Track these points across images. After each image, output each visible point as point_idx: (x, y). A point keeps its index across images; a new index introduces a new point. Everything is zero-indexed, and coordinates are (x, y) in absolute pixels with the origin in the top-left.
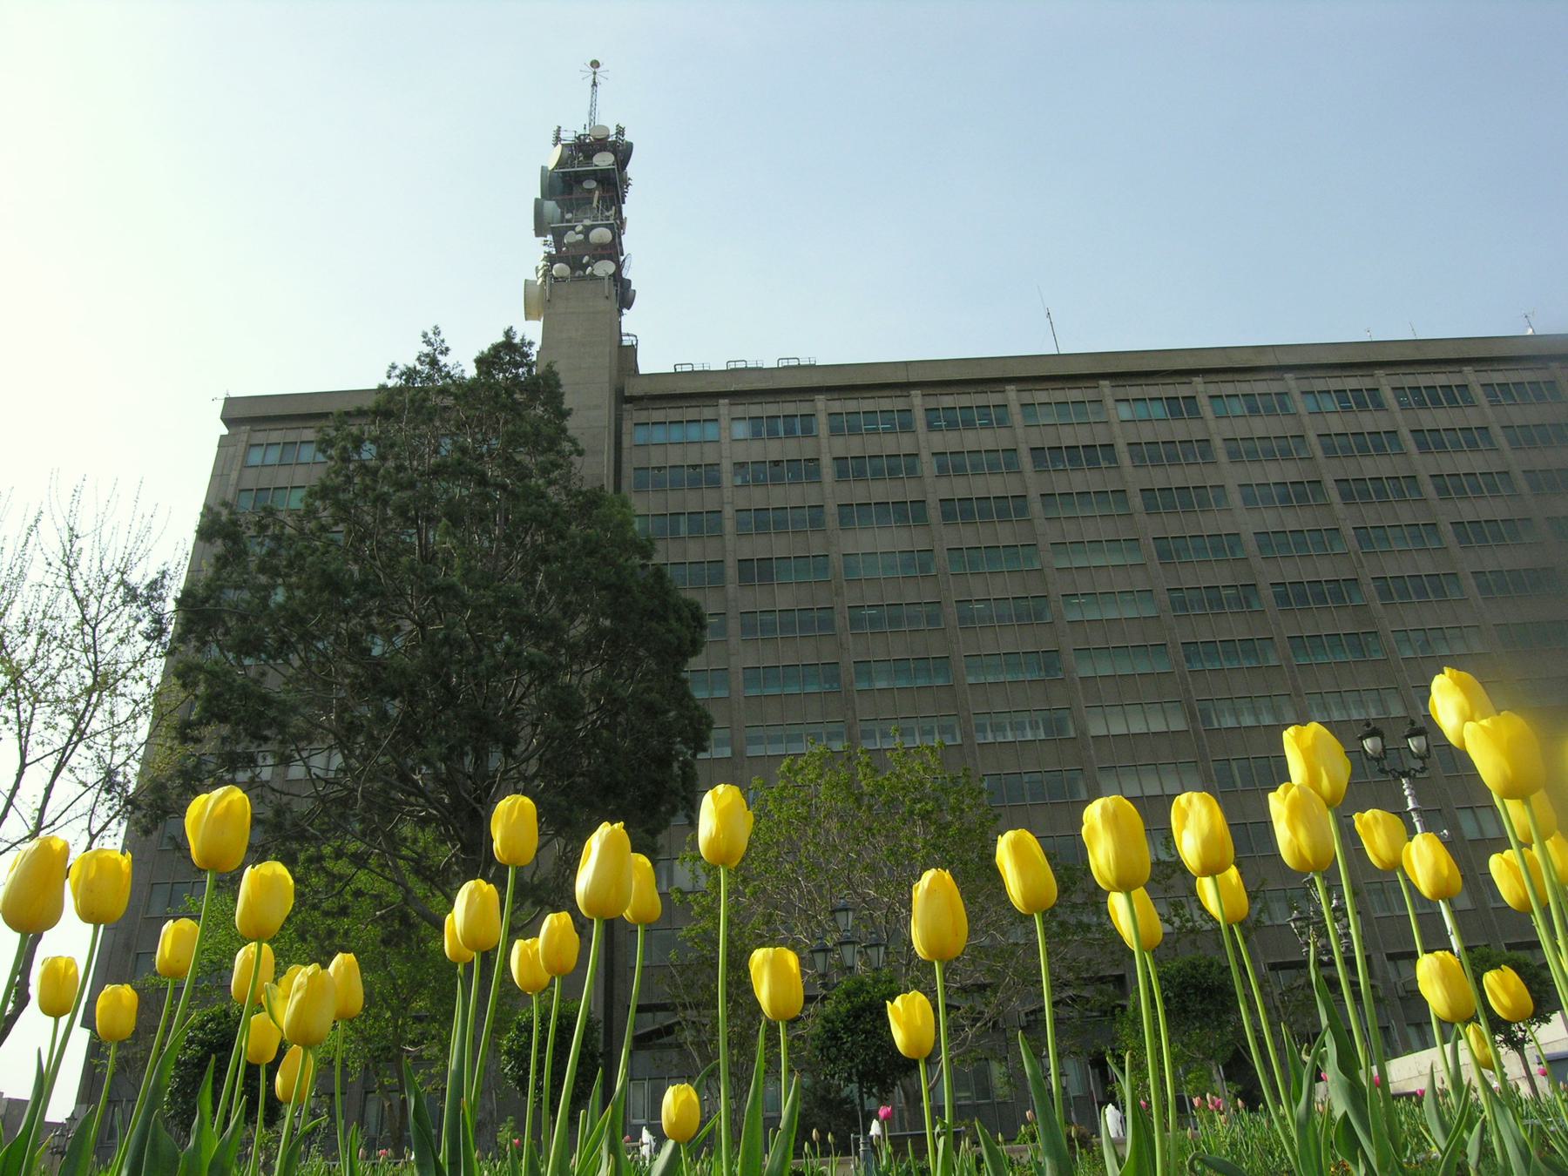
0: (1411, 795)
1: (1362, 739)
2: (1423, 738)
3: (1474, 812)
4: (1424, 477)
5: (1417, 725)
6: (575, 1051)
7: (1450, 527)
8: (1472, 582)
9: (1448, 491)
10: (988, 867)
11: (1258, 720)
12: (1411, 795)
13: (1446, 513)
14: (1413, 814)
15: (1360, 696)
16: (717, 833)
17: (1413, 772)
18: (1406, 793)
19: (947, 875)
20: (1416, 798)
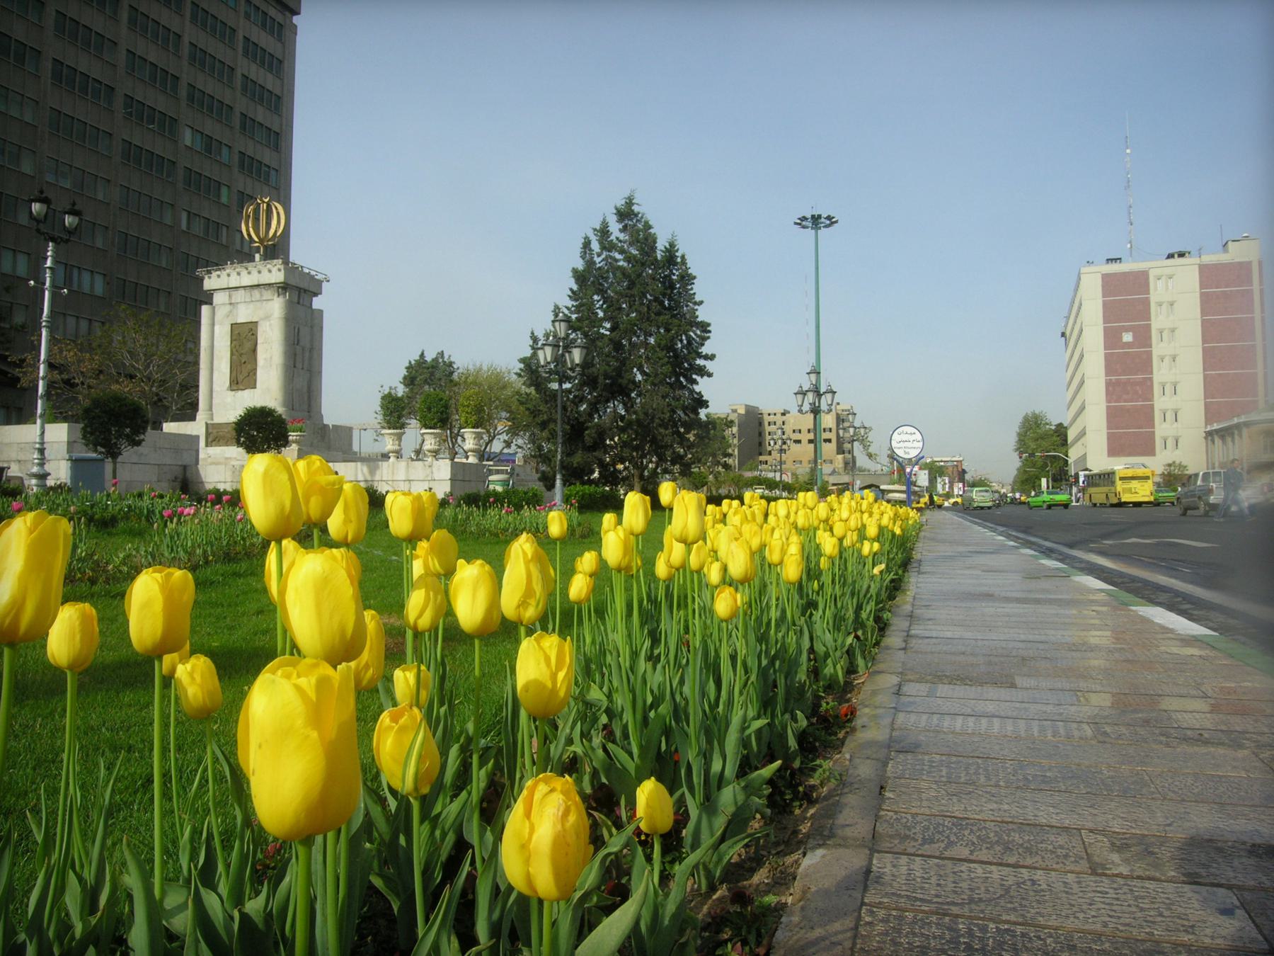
0: (52, 256)
1: (66, 213)
2: (45, 207)
3: (15, 256)
4: (186, 39)
5: (76, 208)
6: (72, 687)
7: (54, 13)
8: (50, 66)
9: (158, 36)
10: (58, 341)
11: (57, 181)
12: (52, 256)
13: (187, 74)
14: (48, 270)
15: (57, 165)
16: (596, 569)
17: (59, 240)
18: (49, 254)
19: (445, 531)
20: (55, 261)
